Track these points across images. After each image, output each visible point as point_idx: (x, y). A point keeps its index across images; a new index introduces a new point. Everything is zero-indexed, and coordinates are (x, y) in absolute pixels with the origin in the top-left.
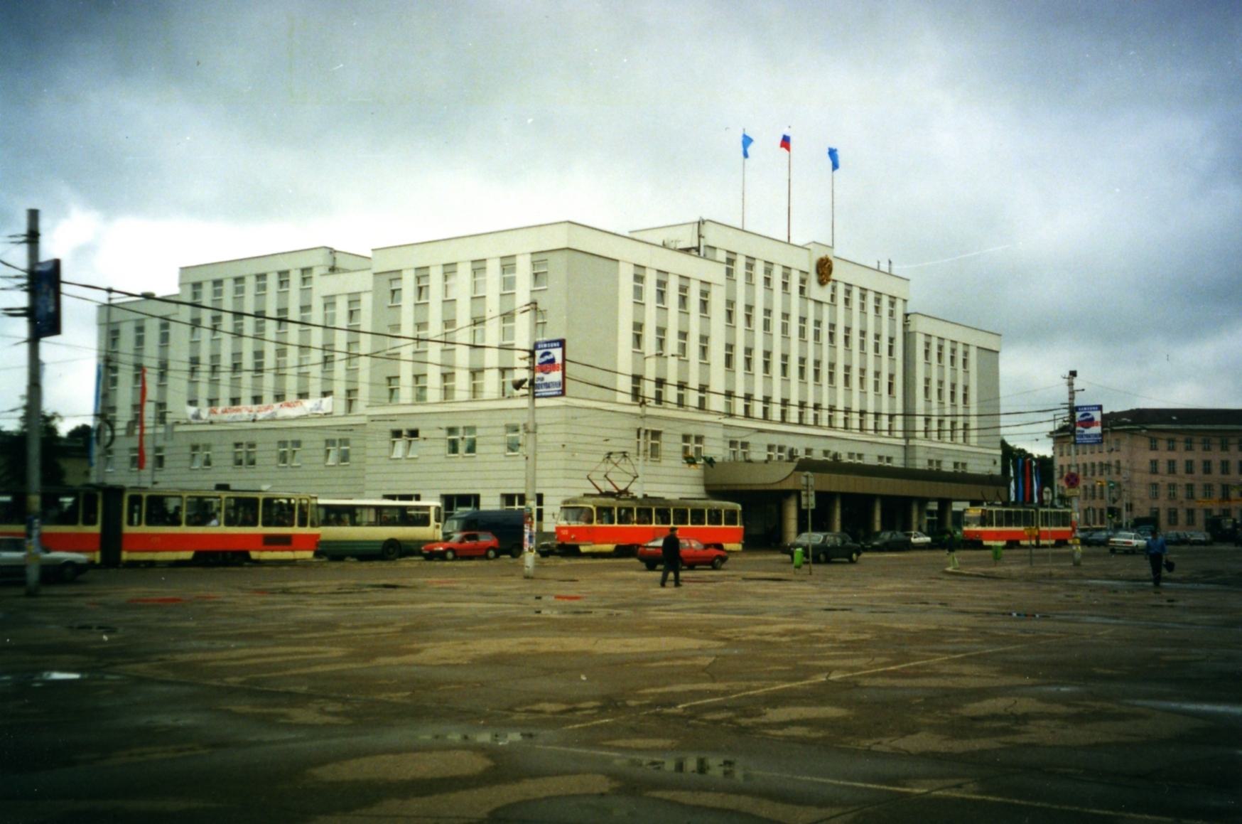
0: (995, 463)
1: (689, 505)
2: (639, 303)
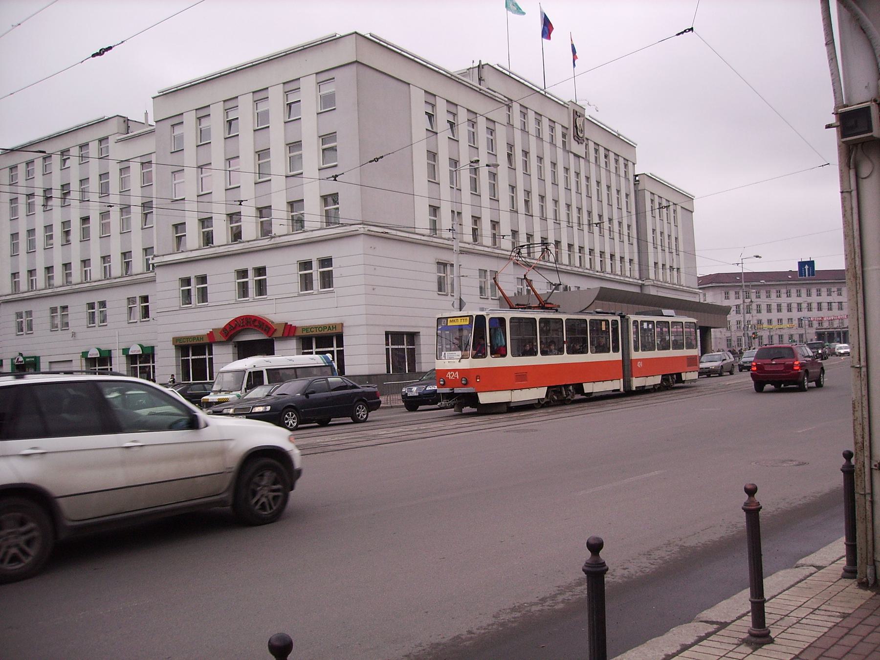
2: (433, 180)
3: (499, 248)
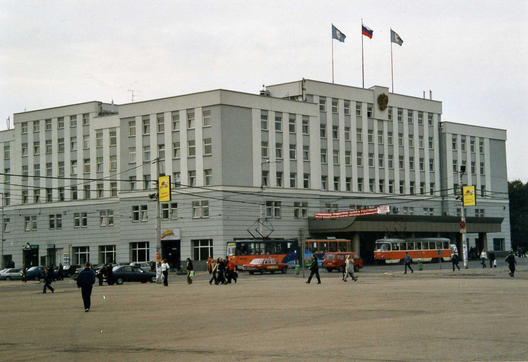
0: (504, 208)
1: (428, 241)
3: (328, 191)
